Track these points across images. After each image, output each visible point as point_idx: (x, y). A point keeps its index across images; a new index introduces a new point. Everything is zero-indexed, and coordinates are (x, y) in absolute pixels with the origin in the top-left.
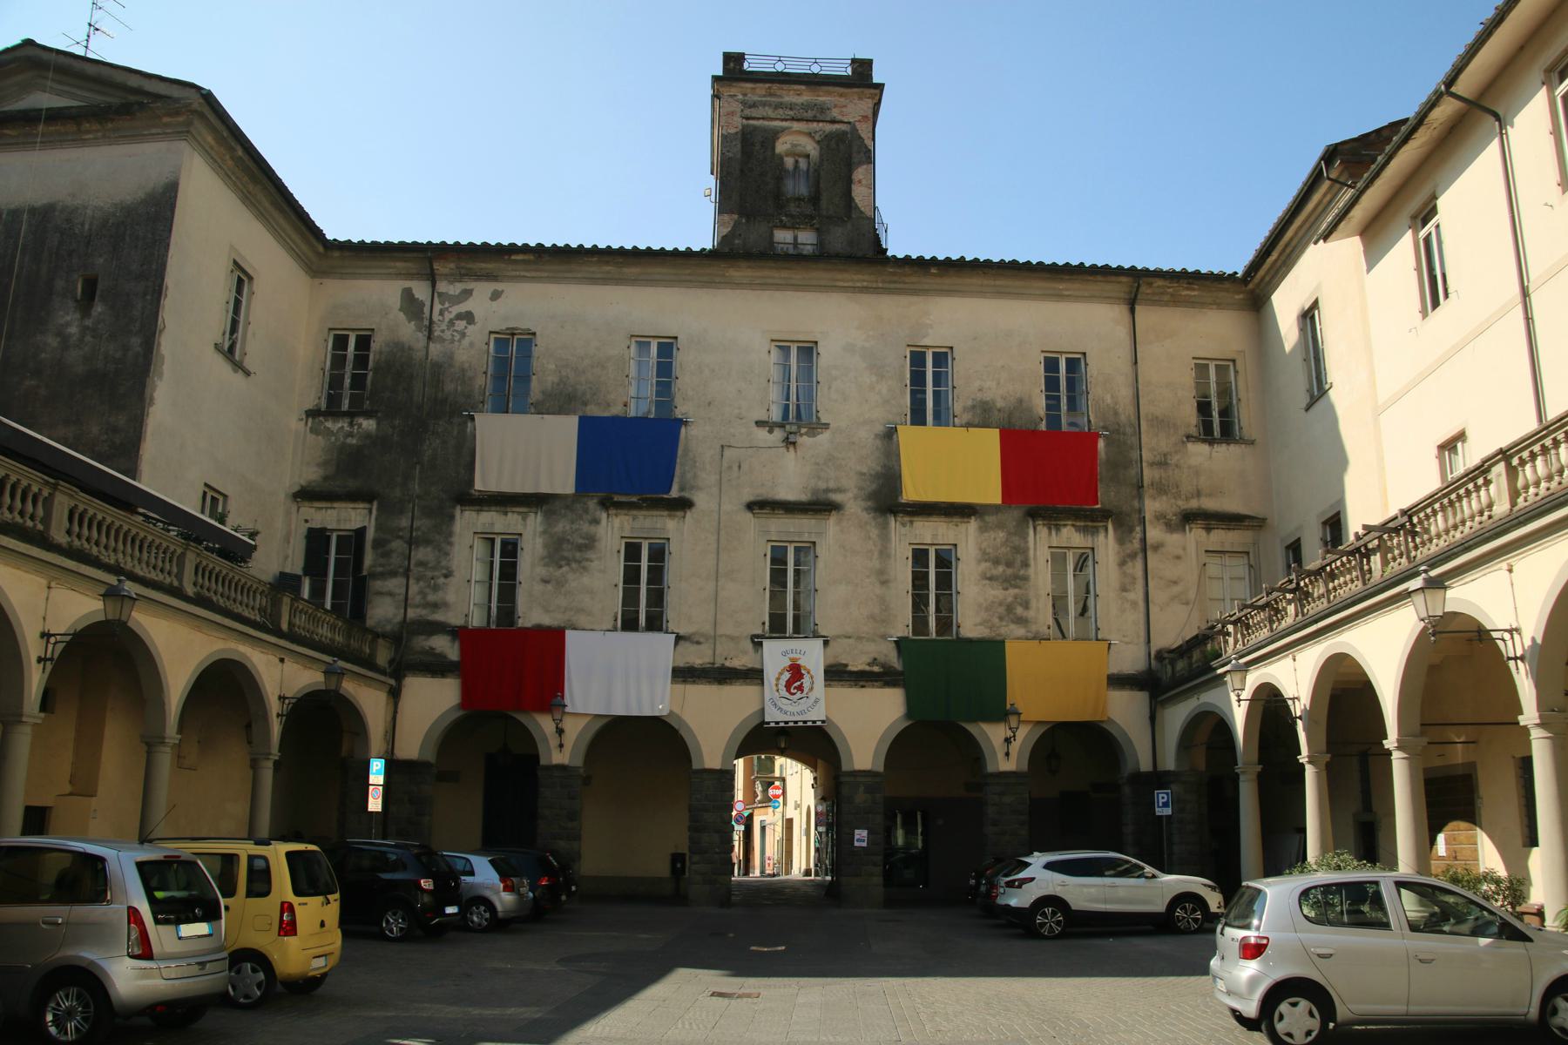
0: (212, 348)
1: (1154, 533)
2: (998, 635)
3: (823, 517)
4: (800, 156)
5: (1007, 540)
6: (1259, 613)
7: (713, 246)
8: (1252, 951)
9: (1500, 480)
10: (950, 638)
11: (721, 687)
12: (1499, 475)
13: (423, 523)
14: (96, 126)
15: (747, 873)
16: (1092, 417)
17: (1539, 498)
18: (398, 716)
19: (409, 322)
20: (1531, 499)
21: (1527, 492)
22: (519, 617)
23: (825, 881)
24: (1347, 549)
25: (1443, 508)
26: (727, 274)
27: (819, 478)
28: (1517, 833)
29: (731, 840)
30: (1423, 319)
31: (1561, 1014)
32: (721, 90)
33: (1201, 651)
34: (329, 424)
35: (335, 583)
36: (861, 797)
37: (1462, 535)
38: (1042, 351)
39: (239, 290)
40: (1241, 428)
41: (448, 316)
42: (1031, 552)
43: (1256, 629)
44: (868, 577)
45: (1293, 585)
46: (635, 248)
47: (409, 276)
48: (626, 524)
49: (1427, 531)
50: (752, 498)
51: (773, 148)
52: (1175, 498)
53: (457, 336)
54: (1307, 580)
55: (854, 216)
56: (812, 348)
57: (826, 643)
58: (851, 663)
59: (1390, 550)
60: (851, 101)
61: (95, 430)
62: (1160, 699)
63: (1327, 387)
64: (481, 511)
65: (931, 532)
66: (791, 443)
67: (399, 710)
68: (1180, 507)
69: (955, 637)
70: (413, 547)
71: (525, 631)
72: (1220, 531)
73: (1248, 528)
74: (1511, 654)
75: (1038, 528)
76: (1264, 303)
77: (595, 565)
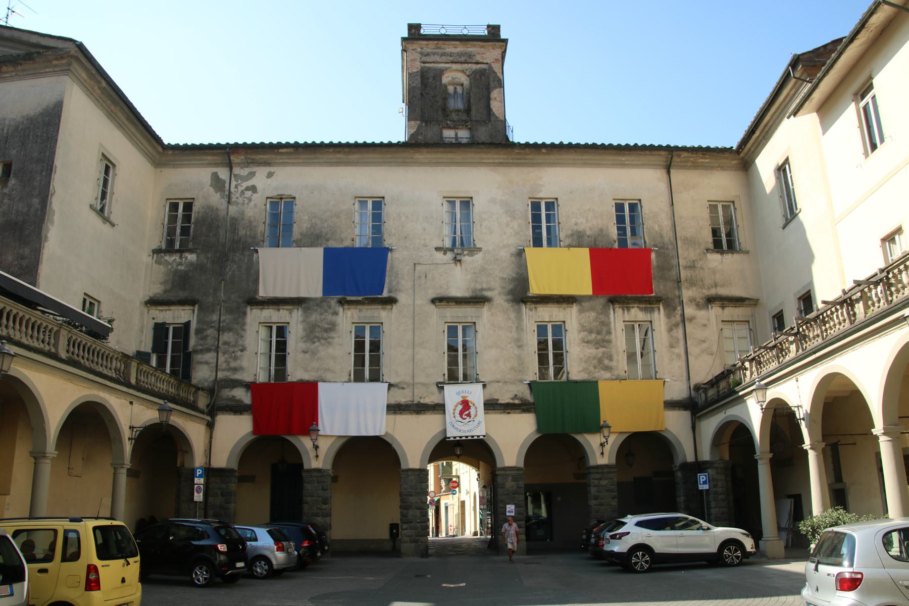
0: (88, 207)
1: (689, 311)
2: (594, 378)
3: (479, 306)
5: (597, 318)
6: (768, 353)
11: (418, 416)
14: (11, 69)
15: (437, 535)
16: (646, 238)
17: (880, 309)
18: (213, 440)
21: (835, 328)
22: (289, 375)
23: (487, 539)
26: (414, 157)
29: (426, 514)
30: (866, 158)
32: (407, 46)
33: (726, 382)
34: (167, 258)
35: (172, 357)
36: (510, 484)
38: (614, 199)
40: (740, 244)
41: (240, 189)
42: (612, 324)
43: (767, 364)
44: (510, 343)
47: (216, 165)
48: (355, 314)
49: (901, 281)
50: (434, 296)
51: (441, 80)
52: (701, 288)
53: (246, 202)
54: (804, 327)
55: (492, 120)
56: (469, 201)
57: (484, 386)
58: (500, 398)
64: (263, 309)
65: (549, 314)
66: (458, 261)
68: (704, 294)
70: (221, 333)
71: (293, 384)
72: (730, 308)
73: (748, 305)
75: (616, 309)
76: (751, 165)
77: (336, 340)
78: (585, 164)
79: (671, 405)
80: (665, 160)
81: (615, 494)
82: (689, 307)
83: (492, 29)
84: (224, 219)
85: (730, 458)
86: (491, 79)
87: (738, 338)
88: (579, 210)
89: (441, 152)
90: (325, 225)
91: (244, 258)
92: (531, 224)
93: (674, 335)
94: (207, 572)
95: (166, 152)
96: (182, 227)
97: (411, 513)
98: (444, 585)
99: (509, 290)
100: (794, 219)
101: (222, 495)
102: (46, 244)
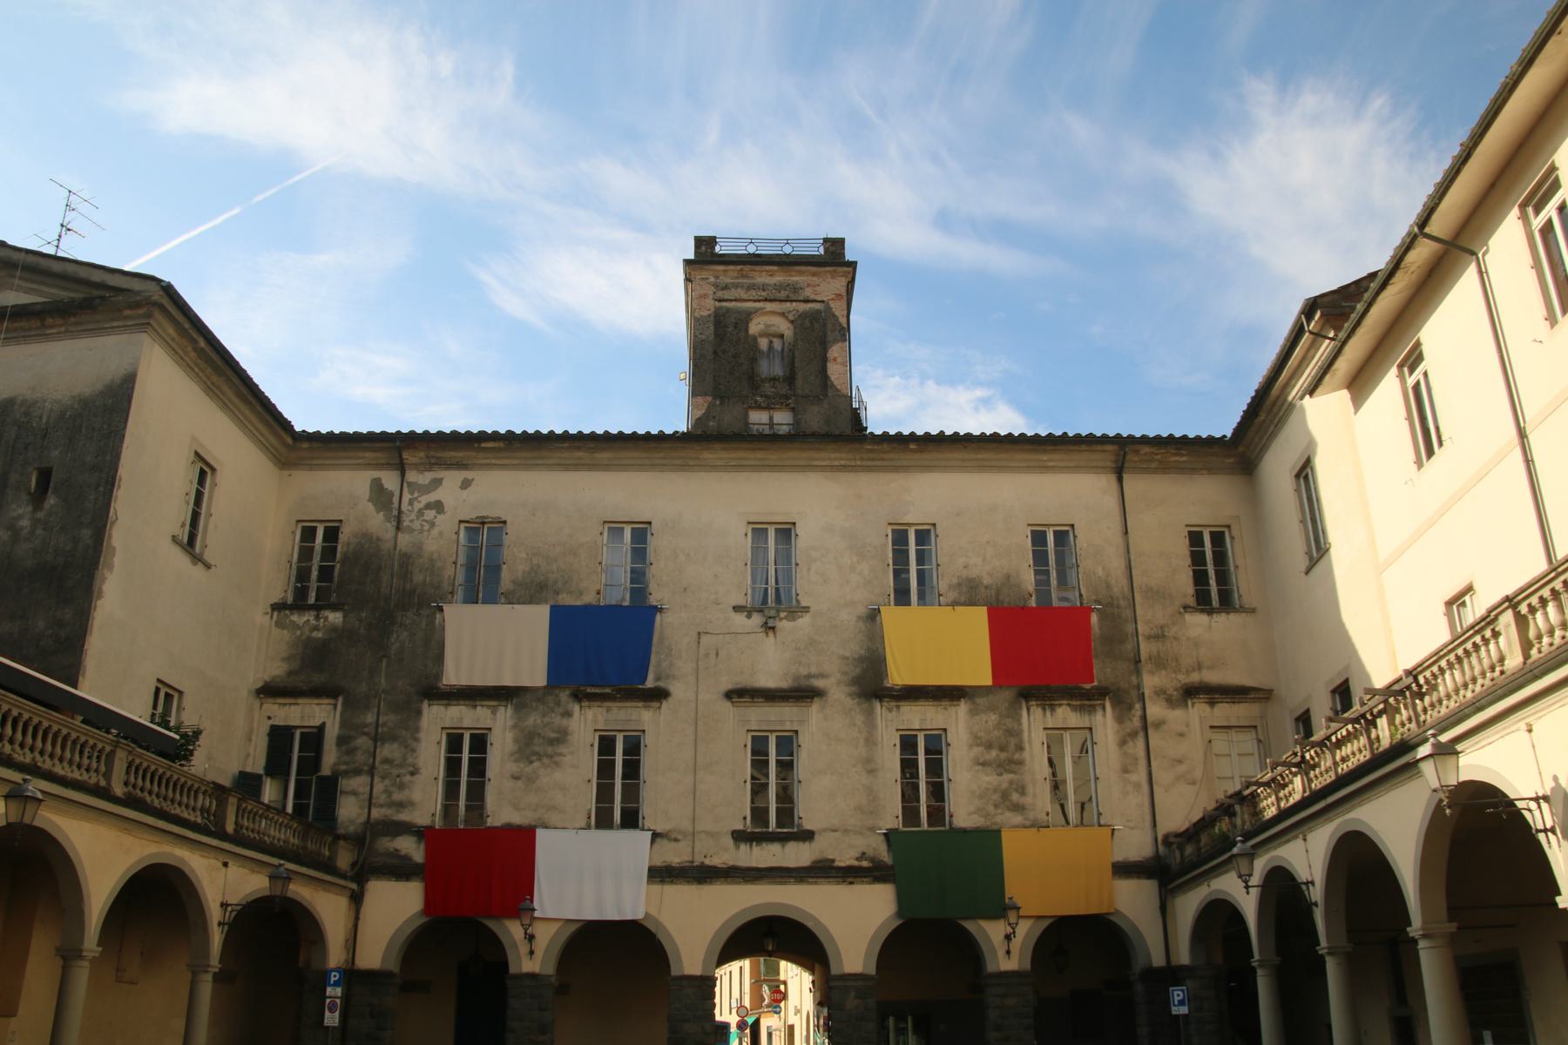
0: (170, 539)
1: (1155, 710)
2: (994, 824)
3: (804, 704)
7: (688, 428)
10: (942, 828)
13: (389, 719)
14: (59, 321)
17: (1554, 647)
18: (360, 922)
19: (378, 513)
20: (1545, 649)
21: (1540, 643)
22: (488, 816)
24: (1352, 716)
26: (701, 457)
34: (295, 618)
37: (1473, 694)
39: (202, 480)
40: (1240, 596)
44: (854, 766)
45: (1298, 759)
46: (606, 432)
48: (600, 717)
50: (730, 687)
51: (747, 330)
52: (1175, 672)
53: (426, 527)
54: (1312, 752)
55: (830, 394)
56: (790, 529)
58: (838, 858)
60: (824, 280)
65: (918, 716)
66: (770, 628)
67: (361, 916)
68: (1180, 682)
69: (947, 827)
70: (379, 744)
73: (1254, 700)
74: (1540, 826)
77: (568, 759)
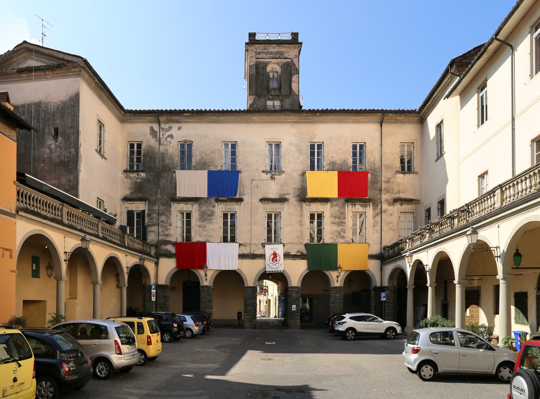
1: (385, 206)
3: (283, 203)
4: (274, 72)
5: (339, 210)
8: (416, 351)
9: (498, 195)
11: (253, 260)
12: (498, 194)
14: (50, 73)
16: (367, 166)
17: (510, 202)
18: (158, 271)
19: (153, 139)
20: (508, 203)
21: (506, 200)
25: (479, 204)
27: (282, 190)
28: (492, 309)
31: (502, 372)
32: (248, 48)
34: (131, 175)
35: (137, 228)
38: (352, 142)
39: (100, 130)
40: (414, 168)
43: (416, 241)
44: (297, 223)
47: (152, 122)
49: (473, 211)
50: (261, 198)
51: (266, 70)
54: (433, 226)
55: (292, 95)
57: (284, 246)
58: (291, 252)
59: (461, 217)
61: (64, 181)
62: (384, 263)
63: (443, 153)
64: (179, 203)
65: (316, 208)
66: (273, 178)
67: (158, 269)
70: (159, 216)
71: (194, 243)
76: (425, 121)
77: (214, 221)
78: (339, 122)
79: (371, 257)
80: (380, 118)
81: (342, 301)
82: (385, 204)
83: (294, 35)
84: (158, 153)
85: (397, 285)
86: (293, 68)
87: (408, 221)
88: (334, 149)
89: (266, 116)
90: (208, 158)
91: (169, 175)
92: (309, 157)
93: (376, 220)
94: (169, 336)
95: (126, 115)
96: (137, 158)
97: (249, 307)
98: (266, 343)
99: (297, 195)
100: (441, 157)
101: (164, 298)
102: (80, 173)
